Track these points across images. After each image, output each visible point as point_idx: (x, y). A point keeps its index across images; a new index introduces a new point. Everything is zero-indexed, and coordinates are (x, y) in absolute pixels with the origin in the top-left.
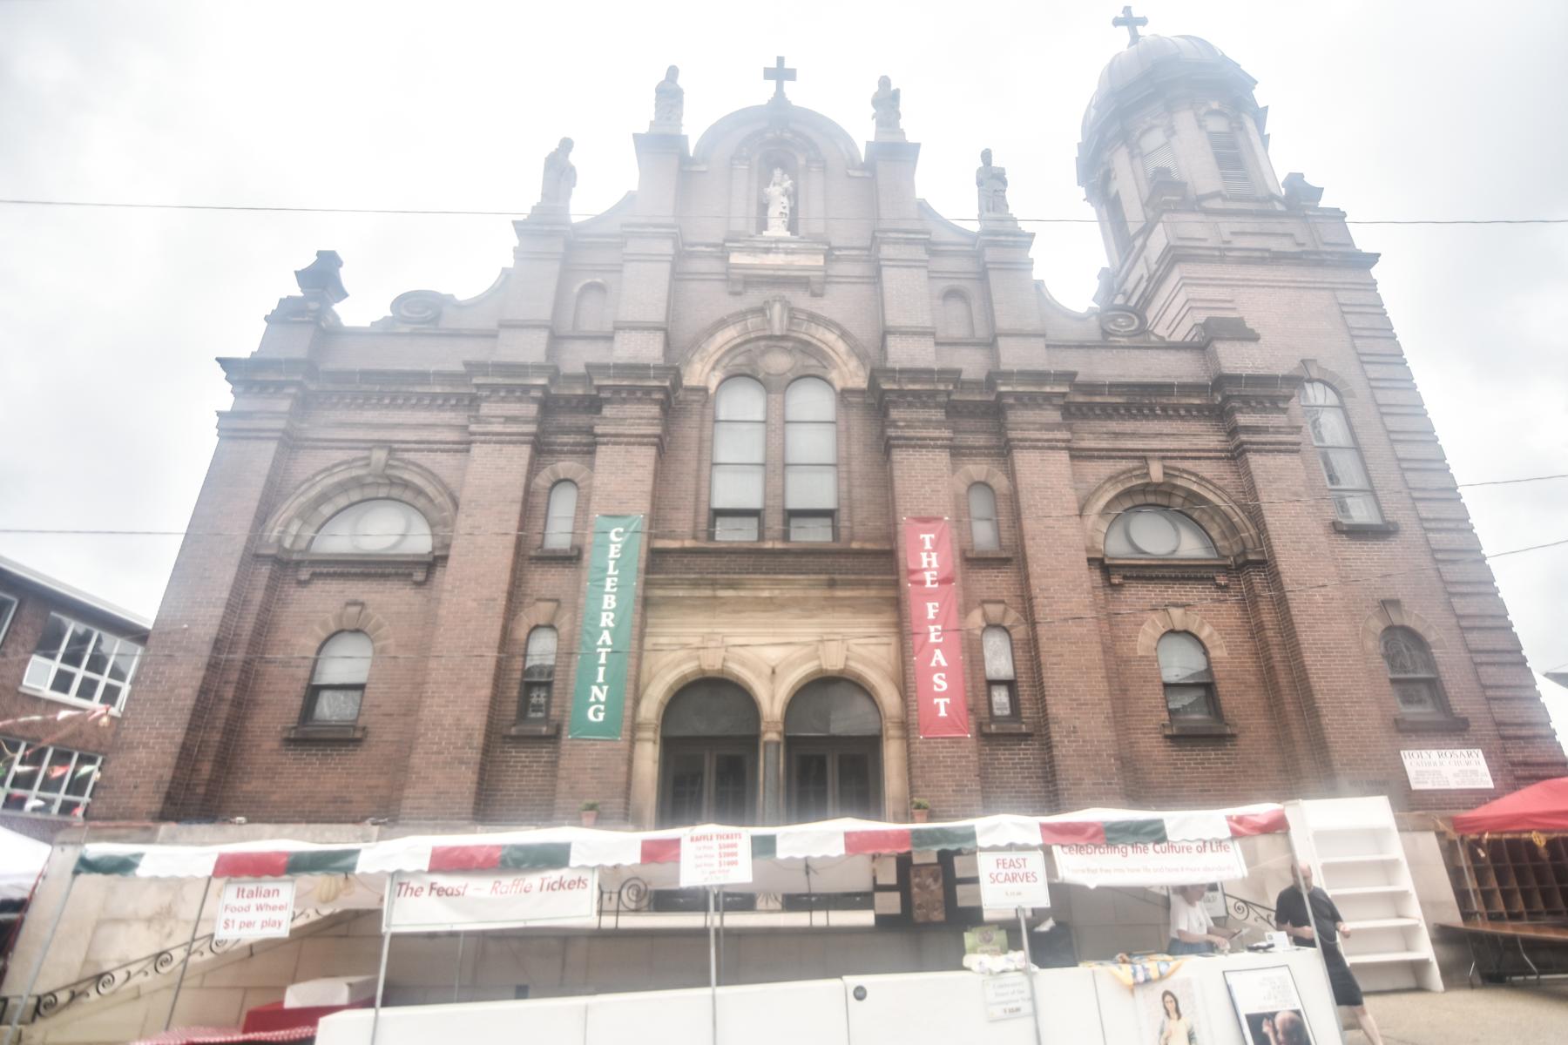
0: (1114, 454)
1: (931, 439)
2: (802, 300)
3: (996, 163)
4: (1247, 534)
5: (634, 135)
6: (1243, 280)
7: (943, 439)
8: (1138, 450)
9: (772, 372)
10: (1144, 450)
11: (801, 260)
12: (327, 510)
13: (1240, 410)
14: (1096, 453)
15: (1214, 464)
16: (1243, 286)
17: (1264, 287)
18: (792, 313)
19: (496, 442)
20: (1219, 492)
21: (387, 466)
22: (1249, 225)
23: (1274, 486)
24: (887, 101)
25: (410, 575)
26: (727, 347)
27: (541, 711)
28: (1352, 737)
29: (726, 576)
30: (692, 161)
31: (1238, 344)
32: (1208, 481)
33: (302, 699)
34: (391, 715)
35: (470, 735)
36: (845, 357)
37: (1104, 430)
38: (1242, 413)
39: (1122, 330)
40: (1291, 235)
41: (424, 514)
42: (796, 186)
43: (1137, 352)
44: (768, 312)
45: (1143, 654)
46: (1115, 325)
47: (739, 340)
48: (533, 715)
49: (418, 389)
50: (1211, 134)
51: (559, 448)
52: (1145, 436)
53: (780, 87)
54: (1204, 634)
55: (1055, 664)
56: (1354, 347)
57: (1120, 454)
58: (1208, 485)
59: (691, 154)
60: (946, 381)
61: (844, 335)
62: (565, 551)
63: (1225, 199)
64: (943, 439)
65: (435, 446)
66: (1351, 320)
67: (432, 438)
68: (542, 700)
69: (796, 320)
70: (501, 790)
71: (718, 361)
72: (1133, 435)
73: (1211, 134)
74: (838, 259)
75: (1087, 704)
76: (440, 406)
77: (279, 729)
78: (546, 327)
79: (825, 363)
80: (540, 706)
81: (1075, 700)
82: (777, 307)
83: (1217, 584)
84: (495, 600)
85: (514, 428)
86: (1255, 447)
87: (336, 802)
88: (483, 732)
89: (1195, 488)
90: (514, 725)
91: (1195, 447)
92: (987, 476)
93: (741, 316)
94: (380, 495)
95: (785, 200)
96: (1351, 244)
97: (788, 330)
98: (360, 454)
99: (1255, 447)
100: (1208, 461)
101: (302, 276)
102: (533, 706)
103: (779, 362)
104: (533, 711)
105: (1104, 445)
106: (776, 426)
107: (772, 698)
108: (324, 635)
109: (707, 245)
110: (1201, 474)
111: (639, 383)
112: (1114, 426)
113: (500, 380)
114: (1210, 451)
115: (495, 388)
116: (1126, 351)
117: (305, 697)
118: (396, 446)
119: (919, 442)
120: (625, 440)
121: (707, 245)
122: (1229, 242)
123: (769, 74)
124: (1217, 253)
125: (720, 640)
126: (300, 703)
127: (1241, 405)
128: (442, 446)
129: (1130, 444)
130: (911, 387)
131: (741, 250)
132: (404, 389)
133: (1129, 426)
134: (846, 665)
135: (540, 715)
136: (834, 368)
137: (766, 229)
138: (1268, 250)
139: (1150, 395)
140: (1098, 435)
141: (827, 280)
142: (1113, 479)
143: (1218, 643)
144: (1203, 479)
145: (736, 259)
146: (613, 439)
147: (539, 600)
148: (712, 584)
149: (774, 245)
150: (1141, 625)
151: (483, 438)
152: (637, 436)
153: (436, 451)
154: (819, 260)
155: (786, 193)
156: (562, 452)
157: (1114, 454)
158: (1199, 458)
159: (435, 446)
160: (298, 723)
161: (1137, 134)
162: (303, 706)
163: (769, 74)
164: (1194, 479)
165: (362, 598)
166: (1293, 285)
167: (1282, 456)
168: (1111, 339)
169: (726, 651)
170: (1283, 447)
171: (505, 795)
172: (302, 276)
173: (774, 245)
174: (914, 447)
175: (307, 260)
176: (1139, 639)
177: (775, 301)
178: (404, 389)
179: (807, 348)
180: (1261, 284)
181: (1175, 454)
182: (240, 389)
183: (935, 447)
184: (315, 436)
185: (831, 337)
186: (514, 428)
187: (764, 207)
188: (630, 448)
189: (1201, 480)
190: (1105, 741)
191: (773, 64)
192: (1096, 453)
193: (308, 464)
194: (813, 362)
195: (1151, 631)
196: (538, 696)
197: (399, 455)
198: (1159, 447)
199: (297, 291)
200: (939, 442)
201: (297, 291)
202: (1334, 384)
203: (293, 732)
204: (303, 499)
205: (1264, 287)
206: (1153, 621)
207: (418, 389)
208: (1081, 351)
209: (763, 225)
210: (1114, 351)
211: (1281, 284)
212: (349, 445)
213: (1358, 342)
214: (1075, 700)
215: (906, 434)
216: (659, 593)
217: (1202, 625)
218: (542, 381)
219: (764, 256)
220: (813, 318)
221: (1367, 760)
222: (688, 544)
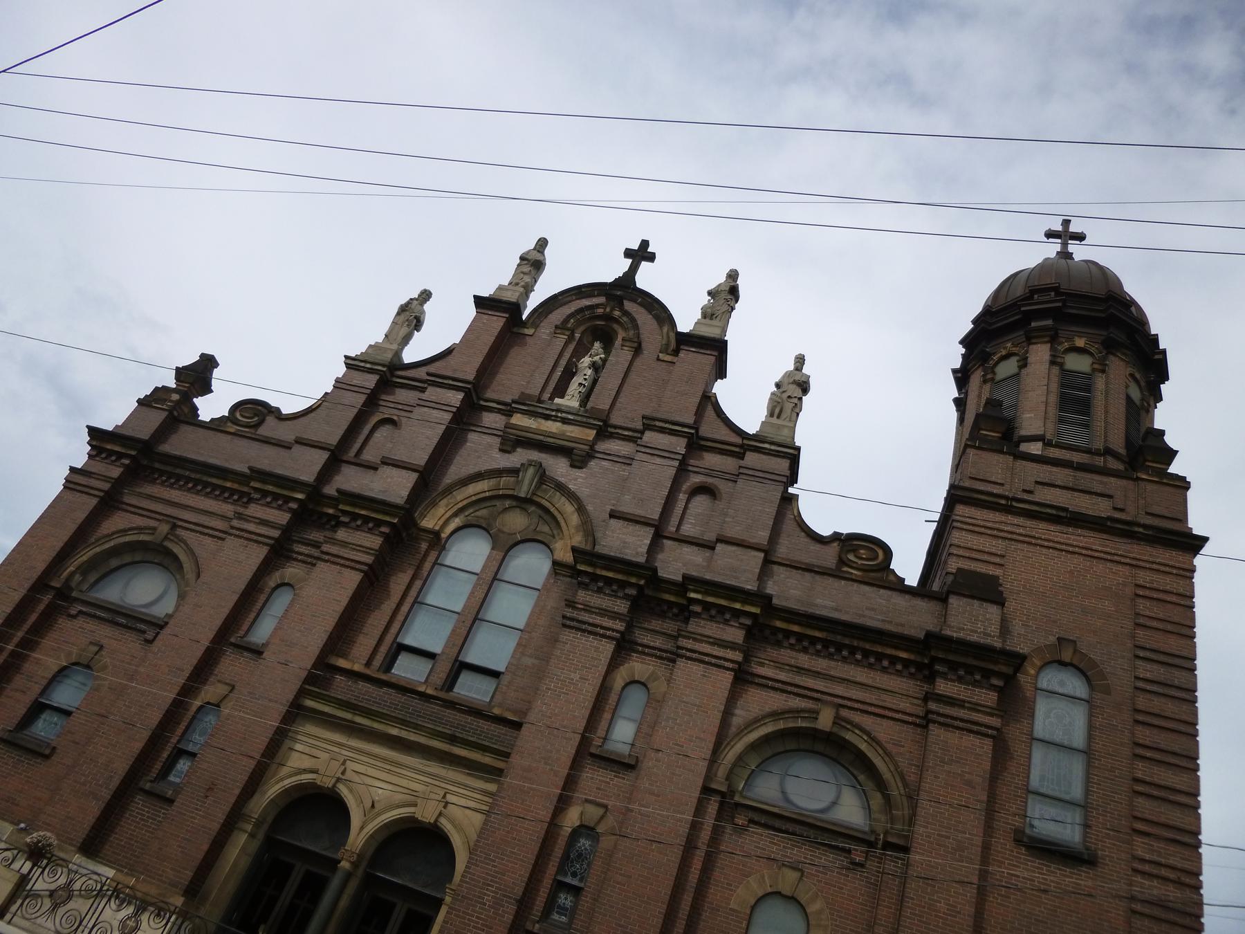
0: (789, 688)
1: (602, 628)
2: (559, 468)
5: (475, 297)
7: (613, 630)
8: (818, 691)
9: (505, 529)
11: (573, 431)
12: (114, 563)
13: (944, 676)
14: (770, 683)
15: (897, 727)
17: (1049, 548)
18: (543, 477)
20: (887, 759)
21: (166, 538)
22: (1061, 475)
23: (946, 768)
26: (474, 498)
29: (41, 607)
30: (524, 324)
31: (976, 603)
32: (878, 743)
33: (25, 710)
34: (78, 743)
35: (111, 777)
36: (573, 531)
37: (793, 662)
38: (946, 679)
39: (860, 562)
40: (1110, 497)
42: (604, 361)
44: (521, 474)
45: (736, 907)
46: (856, 557)
47: (487, 494)
48: (556, 916)
49: (214, 481)
50: (1065, 373)
51: (295, 556)
52: (832, 678)
54: (812, 908)
55: (618, 883)
56: (1133, 637)
57: (796, 690)
58: (878, 748)
59: (524, 317)
60: (640, 576)
61: (581, 509)
62: (258, 646)
66: (1142, 605)
67: (206, 523)
70: (116, 834)
72: (817, 674)
74: (611, 436)
79: (555, 532)
80: (567, 909)
82: (531, 471)
83: (851, 859)
84: (183, 671)
86: (941, 720)
87: (8, 801)
88: (121, 778)
89: (863, 747)
91: (880, 704)
95: (589, 372)
97: (534, 494)
98: (152, 523)
101: (181, 373)
102: (559, 907)
103: (516, 521)
105: (782, 676)
106: (491, 580)
107: (362, 828)
109: (499, 403)
110: (873, 734)
111: (373, 515)
112: (804, 660)
114: (897, 711)
116: (856, 584)
118: (180, 523)
119: (590, 628)
120: (342, 562)
121: (499, 403)
122: (1030, 492)
123: (628, 253)
125: (442, 794)
128: (211, 532)
129: (810, 682)
132: (205, 478)
135: (564, 919)
136: (561, 539)
138: (1065, 510)
142: (775, 715)
144: (874, 739)
145: (518, 420)
146: (333, 559)
147: (219, 681)
149: (554, 413)
151: (238, 533)
152: (353, 561)
154: (591, 434)
155: (594, 366)
156: (296, 560)
157: (789, 688)
159: (206, 531)
160: (14, 729)
163: (628, 253)
165: (104, 642)
166: (1084, 552)
168: (845, 569)
169: (445, 807)
170: (975, 728)
171: (117, 839)
173: (554, 413)
174: (584, 631)
176: (739, 891)
177: (531, 465)
179: (548, 515)
180: (1046, 544)
181: (856, 705)
185: (569, 508)
187: (569, 373)
189: (873, 740)
191: (635, 246)
192: (770, 683)
193: (118, 521)
196: (566, 899)
197: (180, 532)
198: (840, 693)
199: (172, 383)
200: (608, 633)
201: (172, 383)
203: (7, 733)
205: (1049, 548)
206: (763, 877)
207: (214, 481)
209: (561, 391)
210: (843, 582)
212: (353, 564)
213: (1140, 633)
215: (581, 618)
216: (309, 703)
220: (561, 488)
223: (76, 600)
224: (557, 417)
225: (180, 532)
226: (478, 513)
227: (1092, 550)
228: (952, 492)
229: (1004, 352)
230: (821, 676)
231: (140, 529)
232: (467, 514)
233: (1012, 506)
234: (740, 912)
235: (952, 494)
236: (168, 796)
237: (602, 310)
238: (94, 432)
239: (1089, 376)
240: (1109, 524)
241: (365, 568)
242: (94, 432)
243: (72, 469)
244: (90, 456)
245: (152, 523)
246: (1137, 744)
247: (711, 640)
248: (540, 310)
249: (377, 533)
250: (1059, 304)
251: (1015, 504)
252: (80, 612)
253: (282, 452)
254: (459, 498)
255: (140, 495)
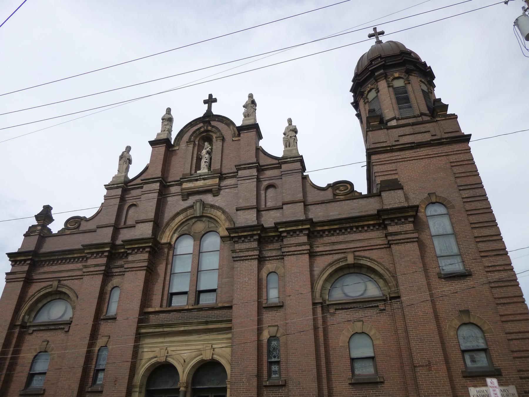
0: (332, 252)
1: (250, 256)
2: (209, 199)
3: (294, 124)
4: (392, 284)
5: (150, 142)
6: (402, 158)
7: (255, 255)
10: (346, 249)
11: (209, 182)
12: (40, 305)
13: (390, 225)
14: (324, 253)
15: (379, 251)
16: (402, 161)
18: (204, 205)
19: (92, 275)
20: (379, 265)
24: (251, 105)
25: (64, 329)
26: (179, 224)
27: (277, 374)
28: (431, 382)
32: (375, 261)
33: (26, 379)
34: (54, 384)
35: (73, 392)
36: (224, 222)
37: (330, 241)
38: (391, 226)
41: (70, 304)
42: (211, 149)
43: (348, 202)
44: (194, 207)
47: (184, 220)
48: (273, 376)
49: (69, 256)
50: (395, 89)
53: (210, 108)
58: (375, 262)
59: (172, 143)
60: (257, 230)
61: (224, 212)
62: (113, 316)
63: (398, 119)
64: (255, 255)
65: (74, 278)
67: (72, 275)
68: (277, 369)
69: (206, 208)
71: (176, 230)
72: (341, 243)
73: (395, 89)
74: (225, 178)
75: (306, 371)
76: (68, 262)
77: (18, 391)
78: (112, 226)
81: (300, 369)
82: (198, 204)
85: (97, 269)
86: (395, 242)
90: (267, 381)
91: (369, 245)
92: (275, 269)
93: (185, 210)
94: (57, 298)
96: (459, 130)
97: (203, 213)
99: (395, 242)
100: (376, 250)
101: (37, 217)
102: (273, 372)
103: (200, 226)
104: (274, 374)
105: (328, 248)
106: (198, 253)
107: (183, 372)
108: (353, 333)
109: (175, 182)
111: (141, 246)
112: (334, 239)
113: (94, 250)
115: (92, 253)
117: (27, 378)
118: (61, 279)
119: (245, 258)
122: (398, 141)
123: (205, 102)
124: (389, 148)
126: (26, 380)
127: (390, 222)
130: (243, 234)
131: (187, 182)
133: (341, 238)
134: (212, 357)
135: (277, 376)
136: (220, 227)
137: (200, 170)
138: (414, 143)
139: (350, 223)
140: (325, 245)
141: (220, 189)
142: (331, 264)
143: (378, 337)
144: (372, 260)
146: (130, 269)
148: (206, 323)
149: (199, 178)
150: (342, 331)
151: (87, 274)
153: (74, 279)
155: (208, 152)
156: (116, 275)
157: (332, 252)
158: (372, 249)
159: (74, 278)
160: (24, 388)
161: (366, 93)
162: (27, 381)
163: (205, 102)
164: (368, 260)
165: (48, 339)
167: (409, 244)
168: (337, 197)
169: (214, 351)
172: (37, 217)
173: (199, 178)
175: (39, 210)
178: (65, 257)
182: (13, 264)
183: (251, 259)
184: (36, 278)
186: (97, 269)
188: (136, 272)
190: (312, 388)
192: (324, 253)
193: (34, 288)
194: (213, 225)
195: (347, 334)
199: (36, 223)
201: (36, 223)
202: (444, 203)
204: (31, 302)
206: (348, 329)
207: (69, 256)
208: (323, 205)
209: (198, 167)
211: (421, 157)
214: (300, 369)
216: (143, 331)
217: (371, 329)
218: (108, 249)
219: (195, 182)
220: (212, 206)
221: (438, 393)
222: (157, 309)
223: (30, 326)
224: (200, 178)
225: (62, 282)
226: (183, 229)
227: (429, 155)
228: (368, 152)
229: (369, 89)
230: (342, 243)
231: (46, 288)
232: (178, 231)
233: (393, 149)
234: (344, 346)
235: (368, 153)
236: (99, 390)
237: (203, 129)
238: (11, 255)
239: (404, 87)
240: (432, 142)
241: (145, 268)
242: (11, 255)
243: (7, 274)
244: (13, 265)
245: (50, 283)
246: (471, 223)
247: (295, 245)
248: (178, 138)
249: (99, 257)
250: (384, 62)
251: (393, 148)
252: (34, 331)
253: (93, 234)
254: (173, 226)
255: (40, 274)
